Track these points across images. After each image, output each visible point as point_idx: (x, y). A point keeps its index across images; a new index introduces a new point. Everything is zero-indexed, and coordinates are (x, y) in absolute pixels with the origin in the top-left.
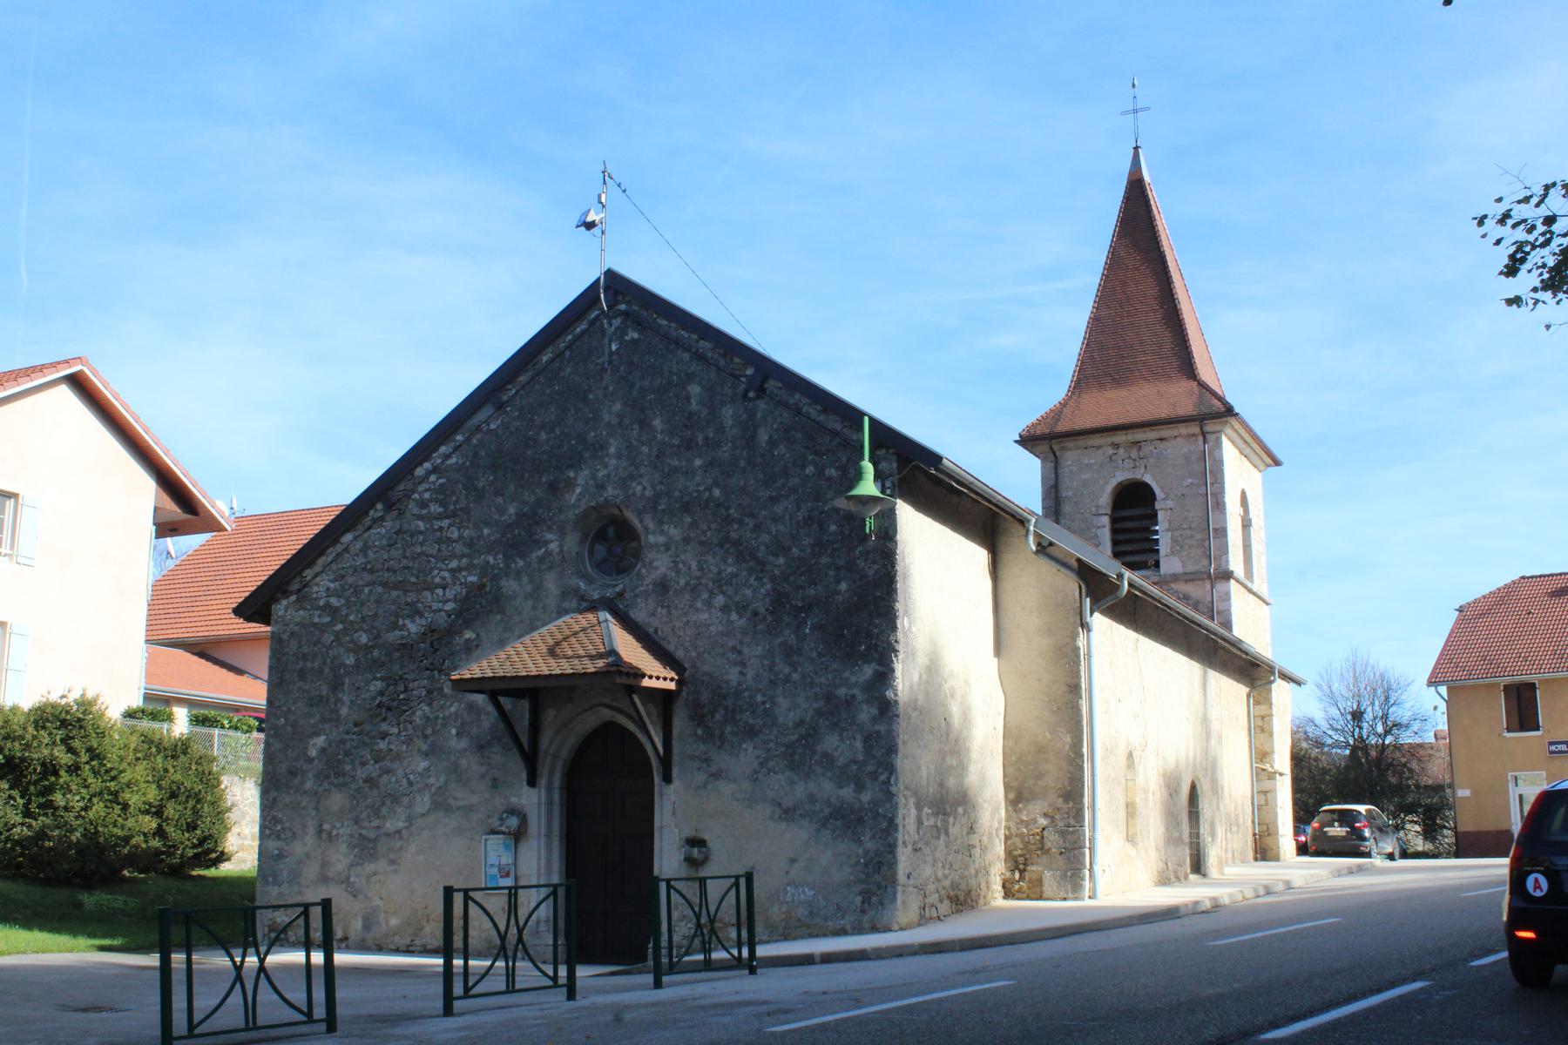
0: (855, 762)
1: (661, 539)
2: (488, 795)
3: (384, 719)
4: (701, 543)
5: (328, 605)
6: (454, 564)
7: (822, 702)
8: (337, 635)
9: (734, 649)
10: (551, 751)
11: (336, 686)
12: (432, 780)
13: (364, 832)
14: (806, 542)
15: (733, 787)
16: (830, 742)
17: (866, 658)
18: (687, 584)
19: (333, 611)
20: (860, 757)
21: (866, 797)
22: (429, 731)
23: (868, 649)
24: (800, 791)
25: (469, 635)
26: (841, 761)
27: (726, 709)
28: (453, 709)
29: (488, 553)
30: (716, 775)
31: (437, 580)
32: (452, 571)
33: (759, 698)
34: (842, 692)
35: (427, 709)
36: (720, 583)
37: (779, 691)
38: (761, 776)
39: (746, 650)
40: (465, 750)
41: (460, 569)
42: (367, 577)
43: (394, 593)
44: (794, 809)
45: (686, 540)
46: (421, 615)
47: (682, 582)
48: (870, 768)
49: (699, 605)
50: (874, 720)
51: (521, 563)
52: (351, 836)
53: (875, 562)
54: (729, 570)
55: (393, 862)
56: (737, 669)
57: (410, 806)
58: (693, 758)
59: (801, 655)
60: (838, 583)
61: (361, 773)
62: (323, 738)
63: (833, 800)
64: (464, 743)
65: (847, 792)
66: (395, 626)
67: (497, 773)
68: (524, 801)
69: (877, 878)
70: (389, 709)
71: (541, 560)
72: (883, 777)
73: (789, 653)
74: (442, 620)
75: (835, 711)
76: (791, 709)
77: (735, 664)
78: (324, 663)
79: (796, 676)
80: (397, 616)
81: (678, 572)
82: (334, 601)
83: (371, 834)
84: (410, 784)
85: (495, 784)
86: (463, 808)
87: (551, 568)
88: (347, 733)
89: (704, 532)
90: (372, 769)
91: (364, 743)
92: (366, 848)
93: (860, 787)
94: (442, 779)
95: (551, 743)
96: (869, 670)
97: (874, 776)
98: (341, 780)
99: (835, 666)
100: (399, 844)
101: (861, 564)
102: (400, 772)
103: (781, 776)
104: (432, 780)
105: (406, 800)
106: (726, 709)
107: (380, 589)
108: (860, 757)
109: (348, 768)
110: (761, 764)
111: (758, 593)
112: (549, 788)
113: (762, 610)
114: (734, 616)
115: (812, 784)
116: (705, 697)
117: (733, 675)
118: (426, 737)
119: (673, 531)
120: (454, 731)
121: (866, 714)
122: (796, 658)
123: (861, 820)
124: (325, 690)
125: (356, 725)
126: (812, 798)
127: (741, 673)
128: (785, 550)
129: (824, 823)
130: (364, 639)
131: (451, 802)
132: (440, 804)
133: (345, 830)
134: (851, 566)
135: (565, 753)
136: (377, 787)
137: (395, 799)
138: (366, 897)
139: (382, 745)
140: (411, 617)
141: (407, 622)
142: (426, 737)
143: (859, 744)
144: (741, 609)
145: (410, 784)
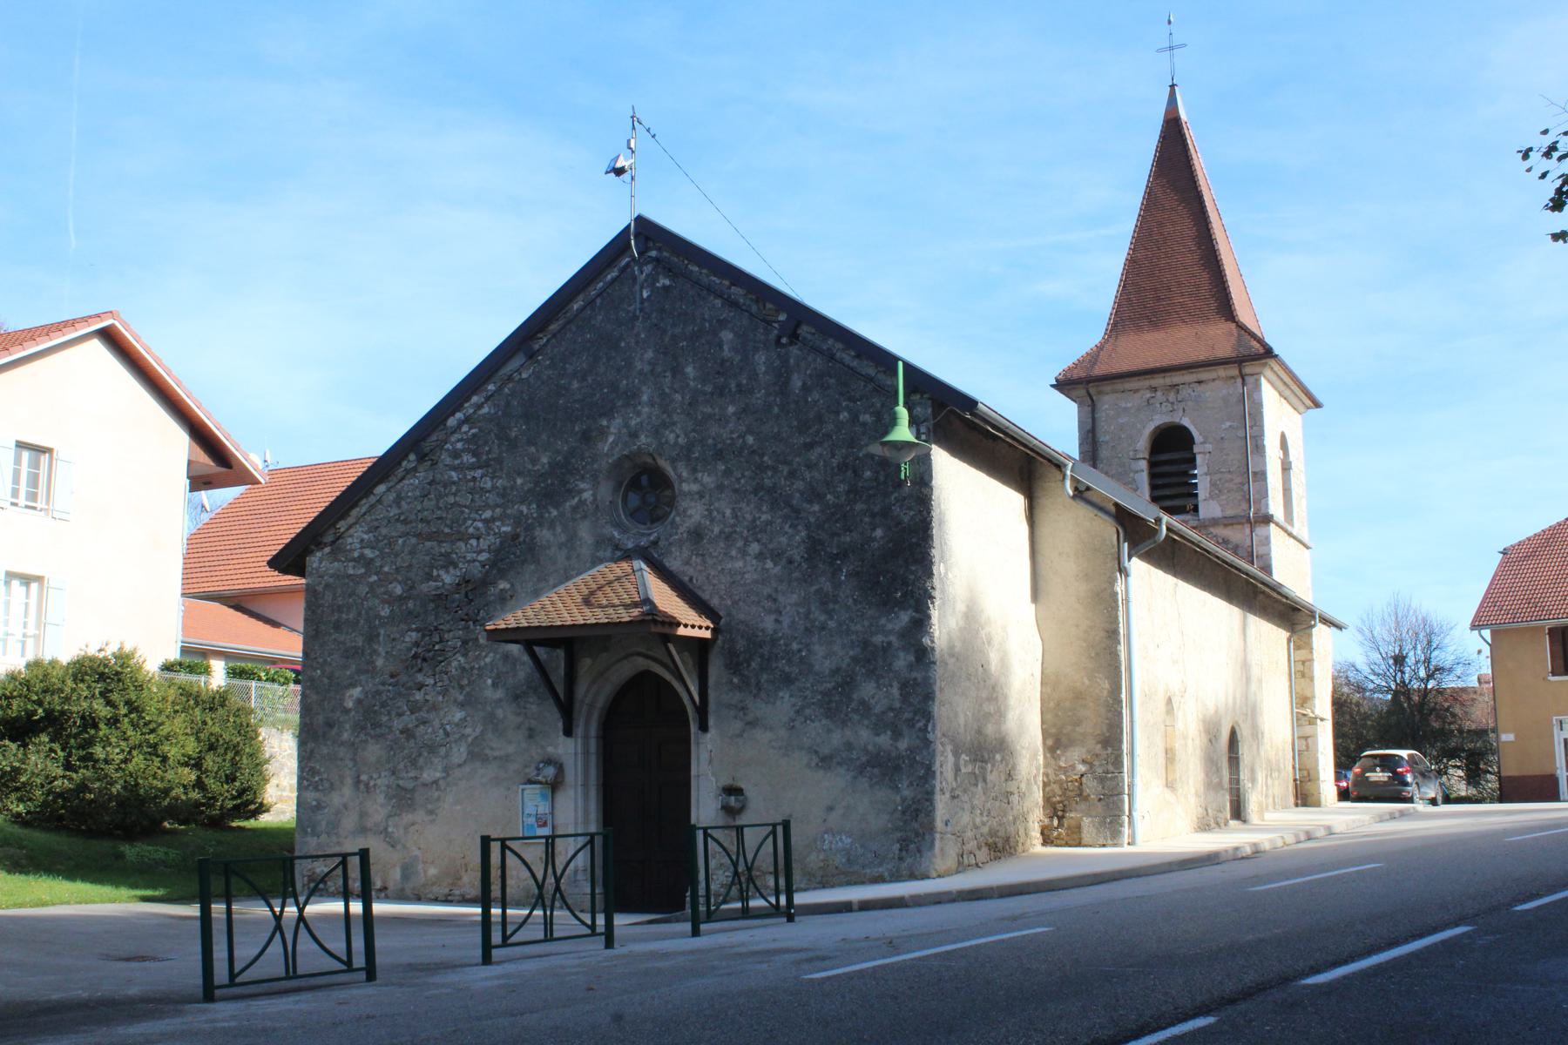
0: (891, 709)
1: (695, 487)
2: (524, 745)
3: (420, 670)
4: (735, 491)
5: (362, 556)
6: (488, 514)
7: (857, 650)
8: (371, 586)
9: (769, 597)
10: (588, 700)
11: (372, 637)
12: (468, 731)
13: (401, 783)
14: (842, 488)
15: (769, 735)
16: (867, 690)
17: (902, 605)
18: (721, 532)
19: (368, 563)
20: (898, 705)
21: (903, 745)
22: (465, 682)
23: (904, 595)
24: (836, 739)
25: (503, 585)
26: (878, 709)
27: (762, 656)
28: (488, 660)
29: (522, 503)
30: (752, 724)
31: (471, 530)
32: (486, 521)
33: (795, 646)
34: (878, 639)
35: (462, 659)
36: (755, 530)
37: (815, 639)
38: (797, 724)
39: (781, 599)
40: (500, 700)
41: (493, 519)
42: (401, 528)
43: (428, 544)
44: (831, 757)
45: (720, 488)
46: (456, 566)
47: (716, 530)
48: (907, 715)
49: (734, 553)
50: (911, 667)
51: (555, 513)
52: (388, 787)
53: (910, 509)
54: (764, 517)
55: (431, 812)
56: (773, 617)
57: (446, 756)
58: (729, 706)
59: (836, 602)
60: (874, 529)
61: (398, 724)
62: (359, 689)
63: (870, 748)
64: (499, 694)
65: (884, 740)
66: (429, 577)
67: (533, 723)
68: (560, 751)
69: (915, 825)
70: (424, 660)
71: (575, 509)
72: (920, 724)
73: (825, 601)
74: (476, 571)
75: (872, 659)
76: (828, 656)
77: (770, 612)
78: (359, 614)
79: (832, 624)
80: (432, 567)
81: (712, 520)
82: (368, 553)
83: (410, 785)
84: (447, 734)
85: (531, 734)
86: (500, 758)
87: (585, 517)
88: (383, 684)
89: (738, 480)
90: (409, 720)
91: (400, 694)
92: (403, 799)
93: (897, 735)
94: (478, 730)
95: (587, 691)
96: (905, 617)
97: (911, 723)
98: (378, 731)
99: (870, 612)
100: (436, 794)
101: (896, 510)
102: (437, 723)
103: (817, 724)
104: (468, 731)
105: (443, 750)
106: (762, 656)
107: (414, 540)
108: (898, 705)
109: (385, 719)
110: (797, 712)
111: (793, 541)
112: (586, 738)
113: (798, 558)
114: (769, 564)
115: (848, 732)
116: (741, 644)
117: (768, 623)
118: (462, 687)
119: (707, 479)
120: (489, 682)
121: (902, 661)
122: (831, 606)
123: (897, 768)
124: (360, 642)
125: (392, 676)
126: (849, 746)
127: (777, 621)
128: (820, 497)
129: (861, 770)
130: (398, 590)
131: (487, 751)
132: (477, 755)
133: (383, 781)
134: (886, 513)
135: (601, 702)
136: (414, 737)
137: (432, 749)
138: (404, 847)
139: (418, 696)
140: (445, 568)
141: (442, 572)
142: (462, 687)
143: (895, 691)
144: (776, 556)
145: (447, 734)
